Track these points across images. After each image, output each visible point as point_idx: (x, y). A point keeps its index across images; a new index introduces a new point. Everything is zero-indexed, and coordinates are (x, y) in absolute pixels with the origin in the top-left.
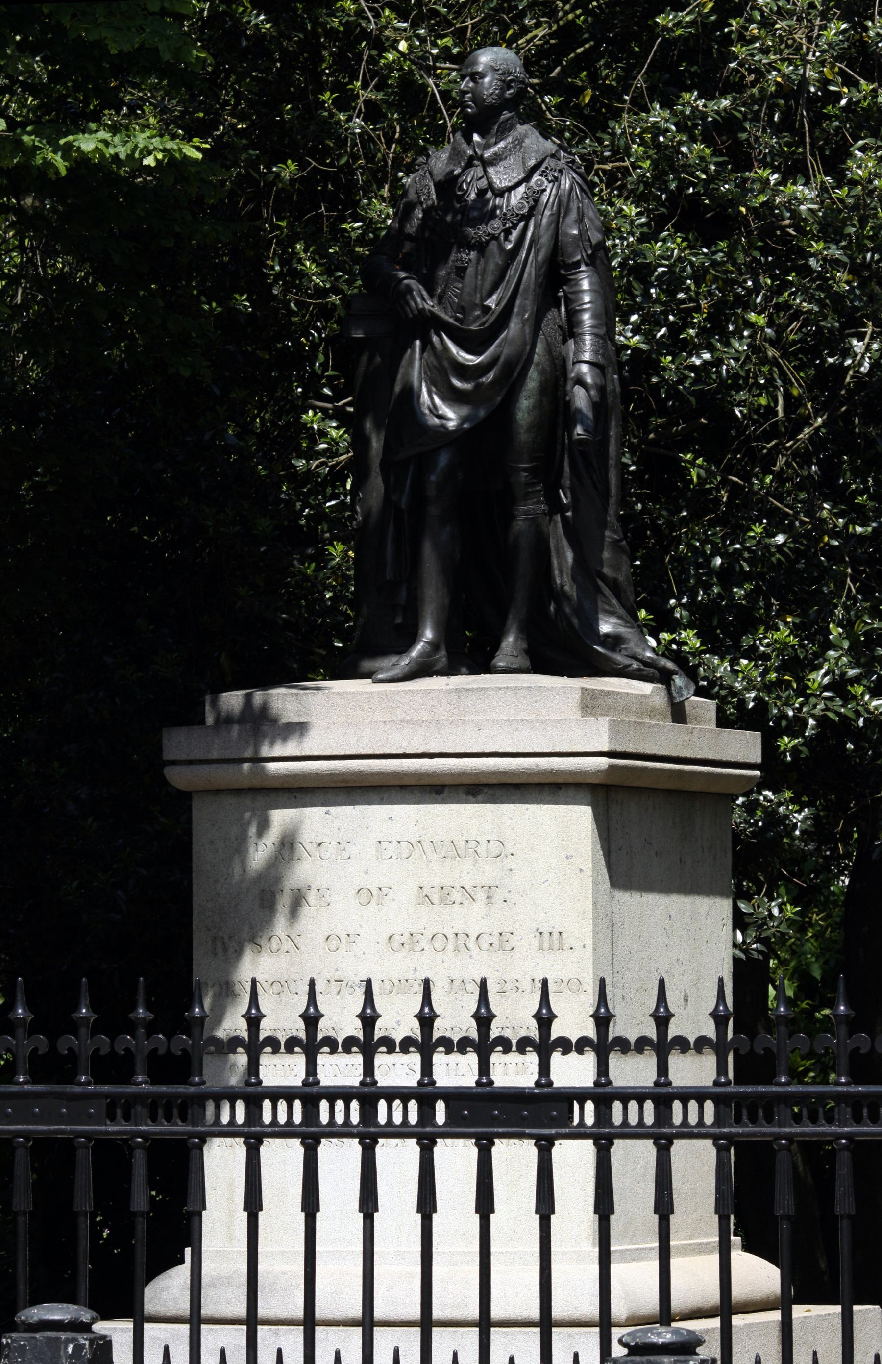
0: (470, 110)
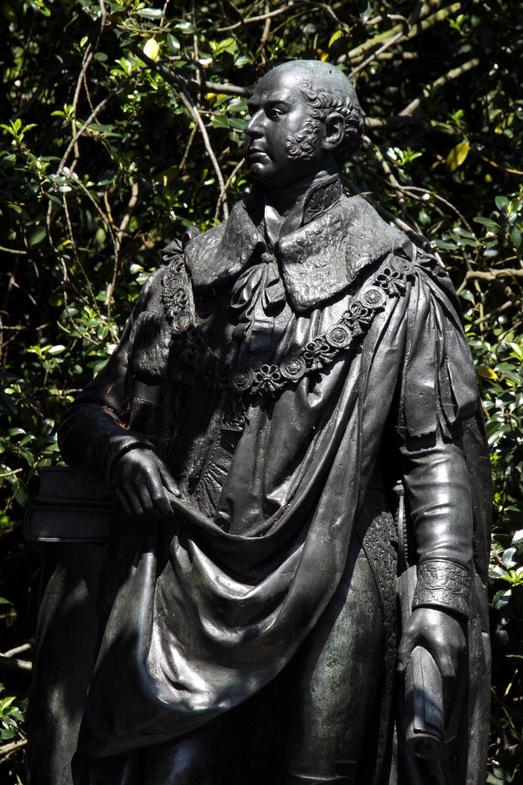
0: (261, 166)
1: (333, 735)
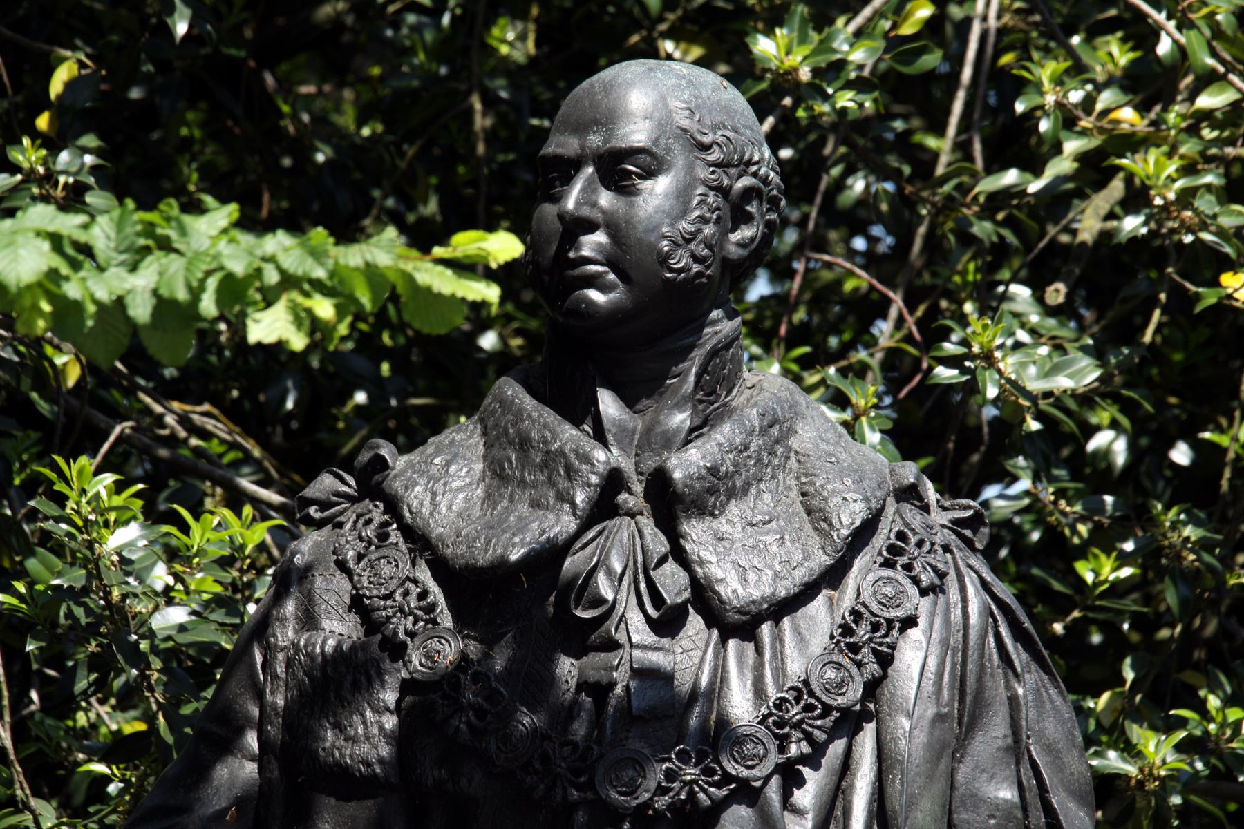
0: (595, 295)
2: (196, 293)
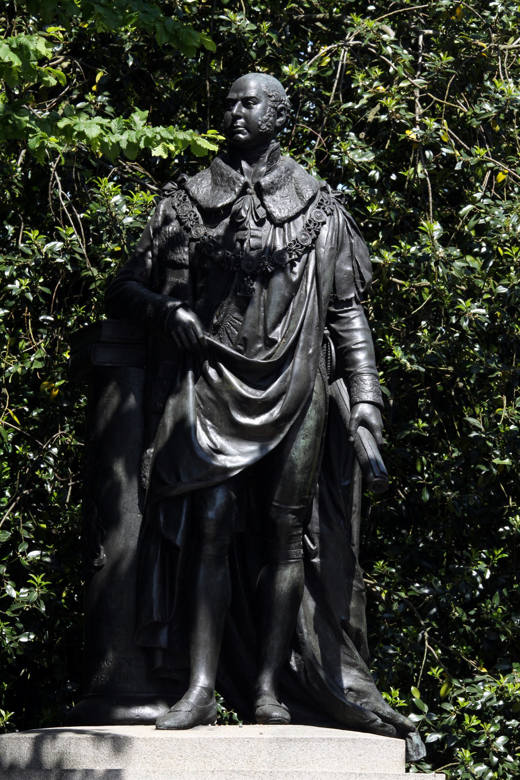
0: (241, 136)
1: (303, 480)
2: (139, 141)
